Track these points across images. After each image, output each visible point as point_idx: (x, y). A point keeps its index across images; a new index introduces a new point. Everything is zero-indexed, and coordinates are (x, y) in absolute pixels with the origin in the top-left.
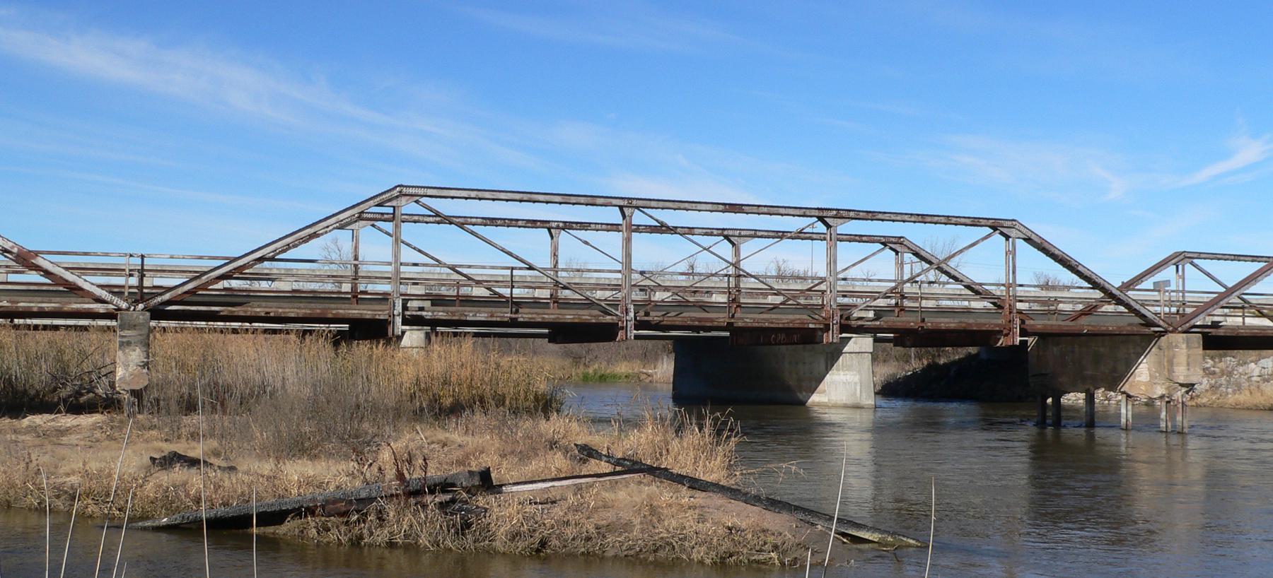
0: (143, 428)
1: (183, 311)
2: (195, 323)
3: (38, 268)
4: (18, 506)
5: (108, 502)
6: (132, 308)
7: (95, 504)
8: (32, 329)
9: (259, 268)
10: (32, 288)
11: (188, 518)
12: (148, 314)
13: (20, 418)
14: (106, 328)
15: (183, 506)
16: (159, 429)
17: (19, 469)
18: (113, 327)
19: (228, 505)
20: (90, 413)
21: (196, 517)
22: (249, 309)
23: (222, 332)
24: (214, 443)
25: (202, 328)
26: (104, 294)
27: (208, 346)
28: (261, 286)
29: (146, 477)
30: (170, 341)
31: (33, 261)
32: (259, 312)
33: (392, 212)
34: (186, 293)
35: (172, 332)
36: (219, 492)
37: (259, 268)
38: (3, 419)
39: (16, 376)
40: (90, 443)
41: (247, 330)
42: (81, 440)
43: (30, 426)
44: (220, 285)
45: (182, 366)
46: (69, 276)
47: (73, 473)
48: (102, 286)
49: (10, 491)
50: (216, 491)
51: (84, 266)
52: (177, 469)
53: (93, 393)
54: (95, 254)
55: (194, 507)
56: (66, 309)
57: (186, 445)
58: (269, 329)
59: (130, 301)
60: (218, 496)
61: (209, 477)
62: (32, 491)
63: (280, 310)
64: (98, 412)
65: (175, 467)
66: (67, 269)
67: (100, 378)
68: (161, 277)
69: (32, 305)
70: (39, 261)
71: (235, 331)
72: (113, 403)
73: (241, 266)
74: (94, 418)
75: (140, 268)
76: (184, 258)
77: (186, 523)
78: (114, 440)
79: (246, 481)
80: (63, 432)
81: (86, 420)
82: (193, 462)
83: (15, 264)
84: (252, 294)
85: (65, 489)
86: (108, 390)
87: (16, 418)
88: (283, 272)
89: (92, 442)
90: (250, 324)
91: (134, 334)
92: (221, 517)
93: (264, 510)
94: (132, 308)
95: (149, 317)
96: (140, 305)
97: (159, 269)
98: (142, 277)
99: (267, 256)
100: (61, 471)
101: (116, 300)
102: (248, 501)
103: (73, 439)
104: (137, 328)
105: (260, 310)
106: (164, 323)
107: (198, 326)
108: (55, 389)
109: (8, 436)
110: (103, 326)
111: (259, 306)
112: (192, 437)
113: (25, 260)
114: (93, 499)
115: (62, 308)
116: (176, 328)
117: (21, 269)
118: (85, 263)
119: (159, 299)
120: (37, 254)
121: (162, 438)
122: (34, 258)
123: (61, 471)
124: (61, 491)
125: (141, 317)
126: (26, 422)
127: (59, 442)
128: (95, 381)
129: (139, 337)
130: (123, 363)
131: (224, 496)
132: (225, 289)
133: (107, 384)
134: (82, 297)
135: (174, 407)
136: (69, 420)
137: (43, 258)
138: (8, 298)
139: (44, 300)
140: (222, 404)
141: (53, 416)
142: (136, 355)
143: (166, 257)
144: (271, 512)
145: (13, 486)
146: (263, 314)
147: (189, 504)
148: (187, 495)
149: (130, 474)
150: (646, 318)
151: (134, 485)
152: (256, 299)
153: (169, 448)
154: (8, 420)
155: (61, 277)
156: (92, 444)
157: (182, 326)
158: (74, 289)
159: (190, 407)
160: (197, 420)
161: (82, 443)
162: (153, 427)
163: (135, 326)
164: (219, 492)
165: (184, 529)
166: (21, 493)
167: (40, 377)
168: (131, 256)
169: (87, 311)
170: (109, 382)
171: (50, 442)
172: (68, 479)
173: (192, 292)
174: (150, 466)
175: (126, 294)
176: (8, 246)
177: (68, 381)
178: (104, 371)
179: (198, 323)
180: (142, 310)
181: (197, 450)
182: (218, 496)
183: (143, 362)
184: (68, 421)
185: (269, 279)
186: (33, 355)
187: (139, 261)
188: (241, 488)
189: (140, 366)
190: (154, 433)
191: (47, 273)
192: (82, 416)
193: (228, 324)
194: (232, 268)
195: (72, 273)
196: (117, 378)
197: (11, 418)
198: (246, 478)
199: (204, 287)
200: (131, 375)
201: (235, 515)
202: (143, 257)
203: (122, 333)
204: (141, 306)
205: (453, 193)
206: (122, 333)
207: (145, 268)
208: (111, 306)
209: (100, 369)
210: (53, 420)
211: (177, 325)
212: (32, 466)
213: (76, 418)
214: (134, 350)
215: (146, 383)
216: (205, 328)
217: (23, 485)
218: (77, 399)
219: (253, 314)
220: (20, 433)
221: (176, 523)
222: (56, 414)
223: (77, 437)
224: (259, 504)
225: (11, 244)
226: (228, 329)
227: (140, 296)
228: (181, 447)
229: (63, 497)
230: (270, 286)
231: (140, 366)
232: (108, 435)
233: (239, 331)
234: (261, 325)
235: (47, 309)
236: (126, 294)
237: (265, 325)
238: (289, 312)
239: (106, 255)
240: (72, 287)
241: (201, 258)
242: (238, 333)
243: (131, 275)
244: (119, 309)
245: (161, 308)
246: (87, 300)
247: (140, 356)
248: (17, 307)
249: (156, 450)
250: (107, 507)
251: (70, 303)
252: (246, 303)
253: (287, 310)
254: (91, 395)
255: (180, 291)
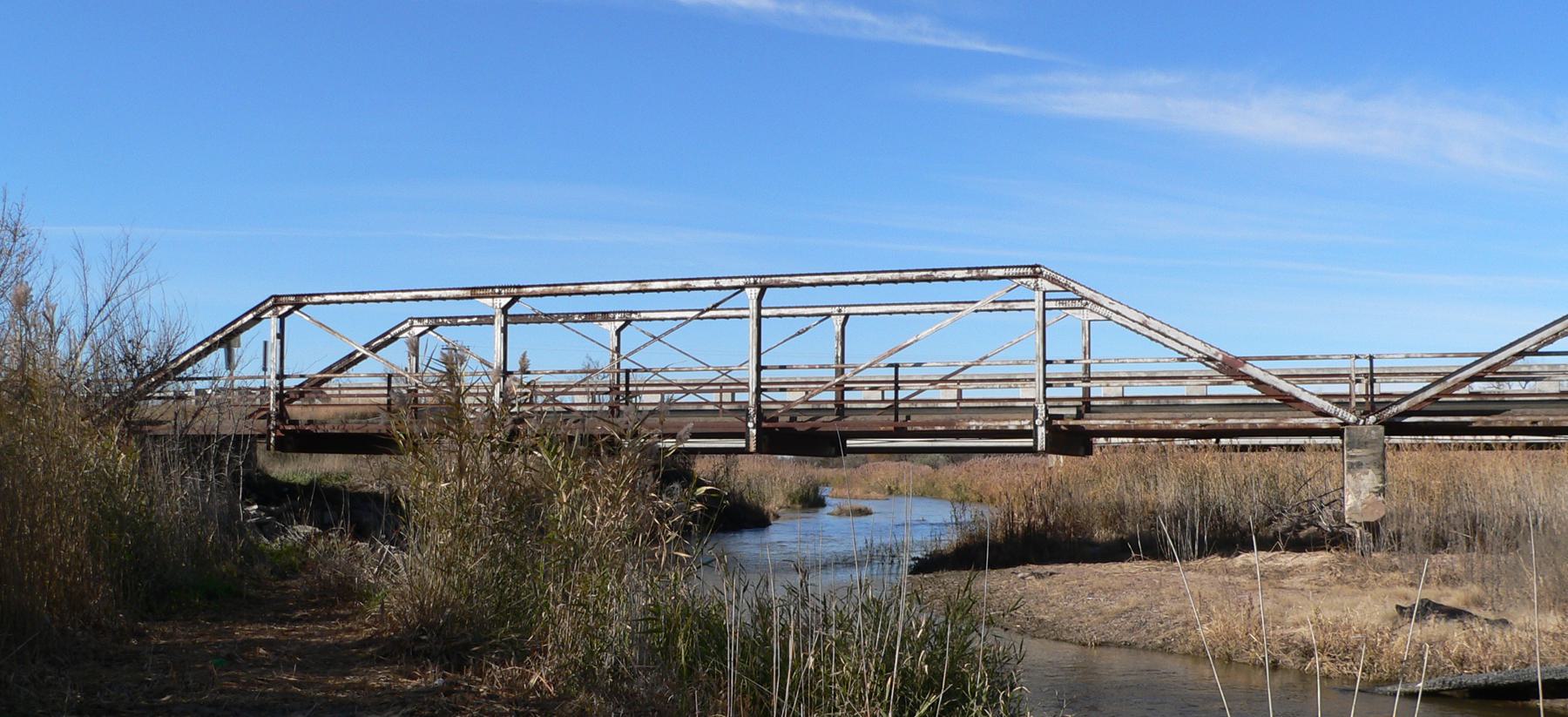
0: (1380, 569)
1: (1425, 423)
2: (1435, 437)
3: (1246, 377)
4: (1240, 660)
5: (1347, 660)
6: (1362, 421)
7: (1332, 662)
8: (1238, 450)
9: (1522, 364)
10: (1236, 401)
11: (1450, 684)
12: (1382, 428)
13: (1233, 556)
14: (1326, 447)
15: (1442, 668)
16: (1402, 570)
17: (1239, 617)
18: (1334, 445)
19: (1501, 669)
20: (1315, 550)
21: (1460, 683)
22: (1510, 418)
23: (1470, 448)
24: (1475, 590)
25: (1445, 444)
26: (1325, 405)
27: (1451, 467)
28: (1513, 388)
29: (1393, 630)
30: (1405, 461)
31: (1241, 369)
32: (1523, 422)
33: (1047, 303)
34: (1427, 400)
35: (1407, 450)
36: (1489, 653)
37: (1522, 364)
38: (1212, 557)
39: (1224, 506)
40: (1317, 587)
41: (1504, 445)
42: (1306, 583)
43: (1244, 566)
44: (1465, 390)
45: (1423, 491)
46: (1284, 386)
47: (1304, 623)
48: (1324, 396)
49: (1229, 643)
50: (1485, 651)
51: (1295, 373)
52: (1432, 621)
53: (1315, 525)
54: (1314, 358)
55: (1456, 670)
56: (1281, 425)
57: (1437, 590)
58: (1532, 444)
59: (1358, 412)
60: (1487, 657)
61: (1474, 632)
62: (1255, 643)
63: (1551, 418)
64: (1324, 549)
65: (1429, 619)
66: (1281, 377)
67: (1322, 507)
68: (1395, 382)
69: (1242, 421)
70: (1248, 369)
71: (1488, 447)
72: (1342, 538)
73: (1496, 364)
74: (1319, 557)
75: (1369, 371)
76: (1422, 357)
77: (1447, 690)
78: (1347, 583)
79: (1524, 638)
80: (1283, 573)
81: (1310, 559)
82: (1452, 613)
83: (1218, 373)
84: (1506, 399)
85: (1295, 642)
86: (1333, 523)
87: (1229, 556)
88: (1546, 369)
89: (1320, 585)
90: (1510, 436)
91: (1364, 453)
92: (1493, 683)
93: (1551, 677)
94: (1362, 421)
95: (1383, 432)
96: (1371, 417)
97: (1386, 372)
98: (897, 389)
99: (1528, 350)
100: (1289, 620)
101: (1341, 412)
102: (1528, 665)
103: (1296, 581)
104: (1369, 445)
105: (1524, 420)
106: (1396, 439)
107: (1440, 442)
108: (1270, 522)
109: (1220, 578)
110: (1321, 445)
111: (1522, 415)
112: (1444, 580)
113: (1231, 369)
114: (1329, 655)
115: (1276, 424)
116: (1412, 444)
117: (1225, 379)
118: (1296, 369)
119: (1395, 409)
120: (1245, 360)
121: (1406, 582)
122: (1242, 366)
123: (1289, 620)
124: (1290, 644)
125: (1373, 432)
126: (1240, 560)
127: (1280, 585)
128: (1317, 512)
129: (1372, 456)
130: (1353, 489)
131: (1495, 658)
132: (1471, 394)
133: (1331, 514)
134: (1299, 410)
135: (1419, 544)
136: (1290, 559)
137: (1252, 365)
138: (1214, 414)
139: (1256, 416)
140: (1482, 540)
141: (1270, 554)
142: (1369, 479)
143: (1400, 356)
144: (1561, 680)
145: (1235, 636)
146: (1528, 424)
147: (1449, 666)
148: (1448, 655)
149: (1373, 626)
150: (791, 425)
151: (1379, 640)
152: (1519, 405)
153: (1418, 595)
154: (1219, 559)
155: (1275, 388)
156: (1321, 588)
157: (1421, 442)
158: (1289, 401)
159: (1439, 543)
160: (1449, 560)
161: (1308, 586)
162: (1395, 568)
163: (1366, 443)
164: (1489, 653)
165: (1445, 696)
166: (1243, 645)
167: (1250, 510)
168: (1357, 357)
169: (1305, 426)
170: (1334, 512)
171: (1269, 585)
172: (1298, 630)
173: (1434, 400)
174: (1396, 617)
175: (1353, 404)
176: (1211, 352)
177: (1284, 512)
178: (1326, 500)
179: (1440, 437)
180: (1374, 424)
181: (1453, 598)
182: (1487, 657)
183: (1378, 487)
184: (1288, 559)
185: (1523, 379)
186: (1241, 482)
187: (1367, 363)
188: (1518, 648)
189: (1374, 492)
190: (1396, 575)
191: (1258, 383)
192: (1304, 554)
193: (1478, 437)
194: (1484, 367)
195: (1287, 382)
196: (1347, 508)
197: (1222, 556)
198: (1523, 635)
199: (1448, 393)
200: (1364, 504)
201: (1512, 682)
202: (1371, 358)
203: (1351, 453)
204: (1372, 419)
205: (375, 296)
206: (1351, 453)
207: (1375, 372)
208: (1336, 420)
209: (1321, 497)
210: (1271, 559)
211: (1413, 441)
212: (1254, 613)
213: (1297, 557)
214: (1367, 474)
215: (1383, 514)
216: (1450, 444)
217: (1245, 636)
218: (1295, 533)
219: (1515, 425)
220: (1233, 574)
221: (1435, 688)
222: (1273, 551)
223: (1302, 579)
224: (1544, 669)
225: (1214, 350)
226: (1479, 444)
227: (1372, 405)
228: (1432, 594)
229: (1293, 652)
230: (1524, 388)
231: (1374, 492)
232: (1338, 578)
233: (1493, 446)
234: (1521, 437)
235: (1259, 426)
236: (1353, 404)
237: (1526, 437)
238: (1562, 421)
239: (1327, 357)
240: (1286, 398)
241: (1444, 356)
242: (1492, 449)
243: (1358, 381)
244: (1346, 424)
245: (1397, 420)
246: (1305, 413)
247: (1373, 480)
248: (1225, 425)
249: (1399, 596)
250: (1346, 666)
251: (1286, 418)
252: (1505, 411)
253: (1561, 418)
254: (1313, 529)
255: (1420, 398)
